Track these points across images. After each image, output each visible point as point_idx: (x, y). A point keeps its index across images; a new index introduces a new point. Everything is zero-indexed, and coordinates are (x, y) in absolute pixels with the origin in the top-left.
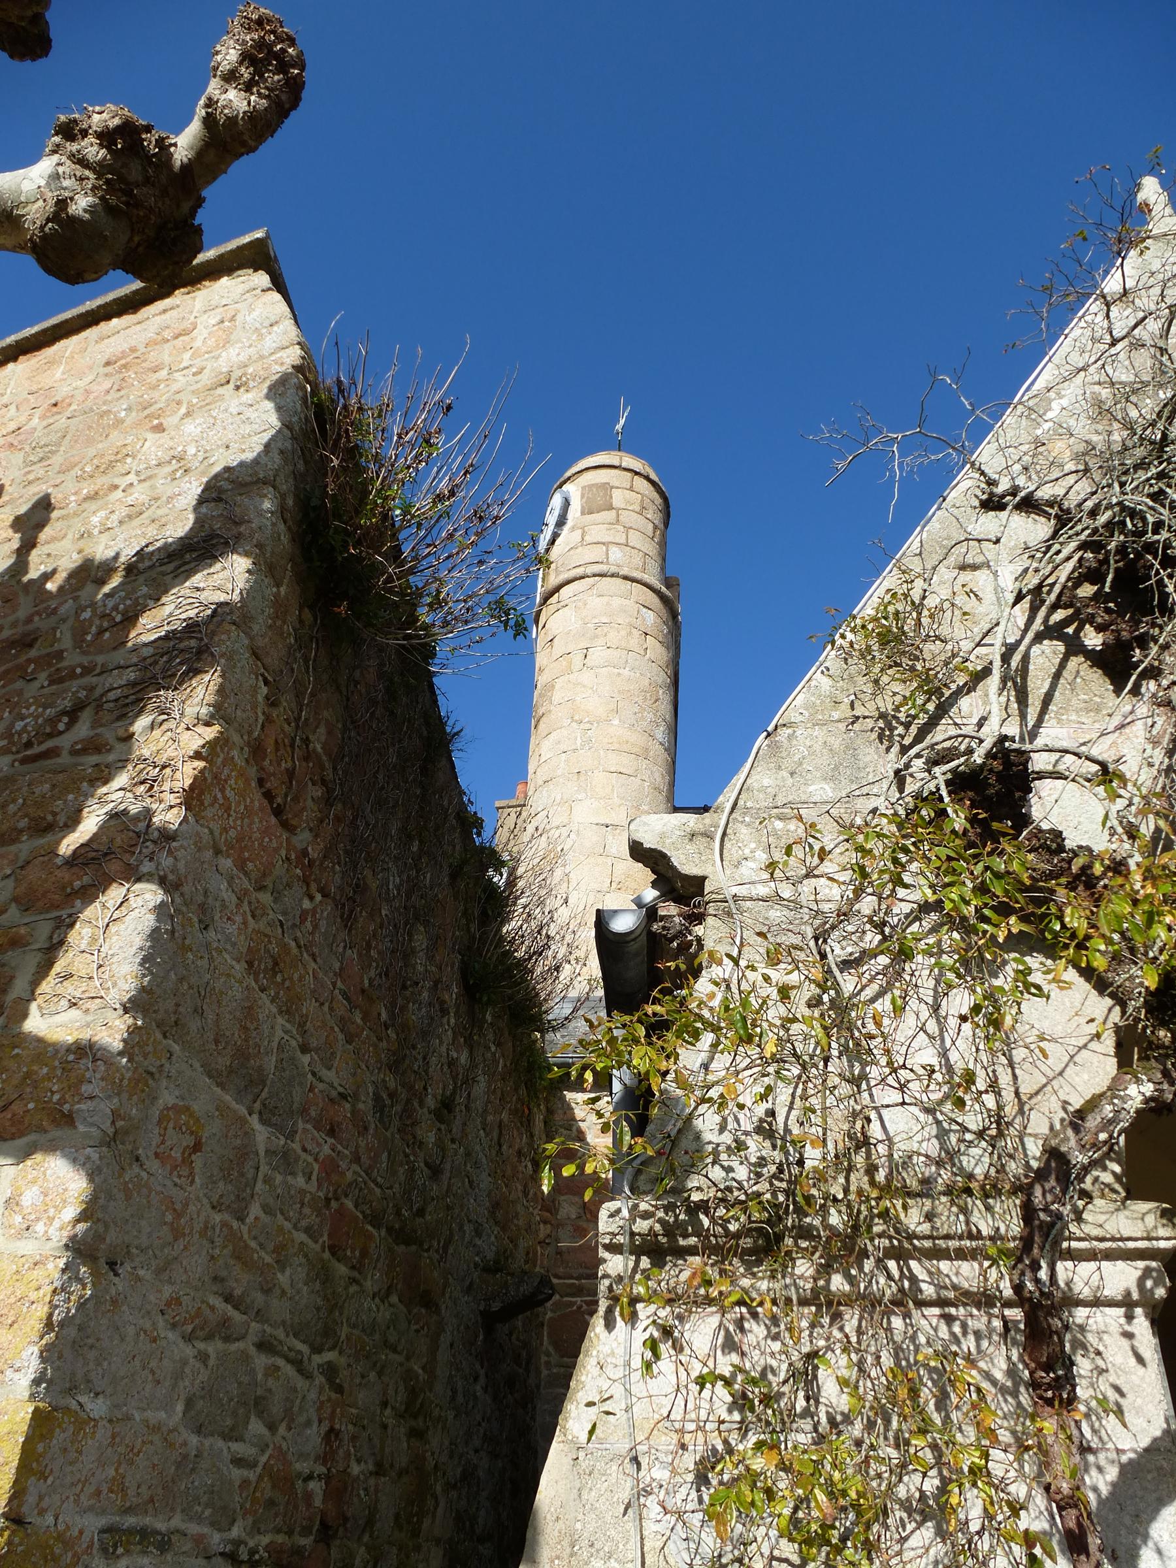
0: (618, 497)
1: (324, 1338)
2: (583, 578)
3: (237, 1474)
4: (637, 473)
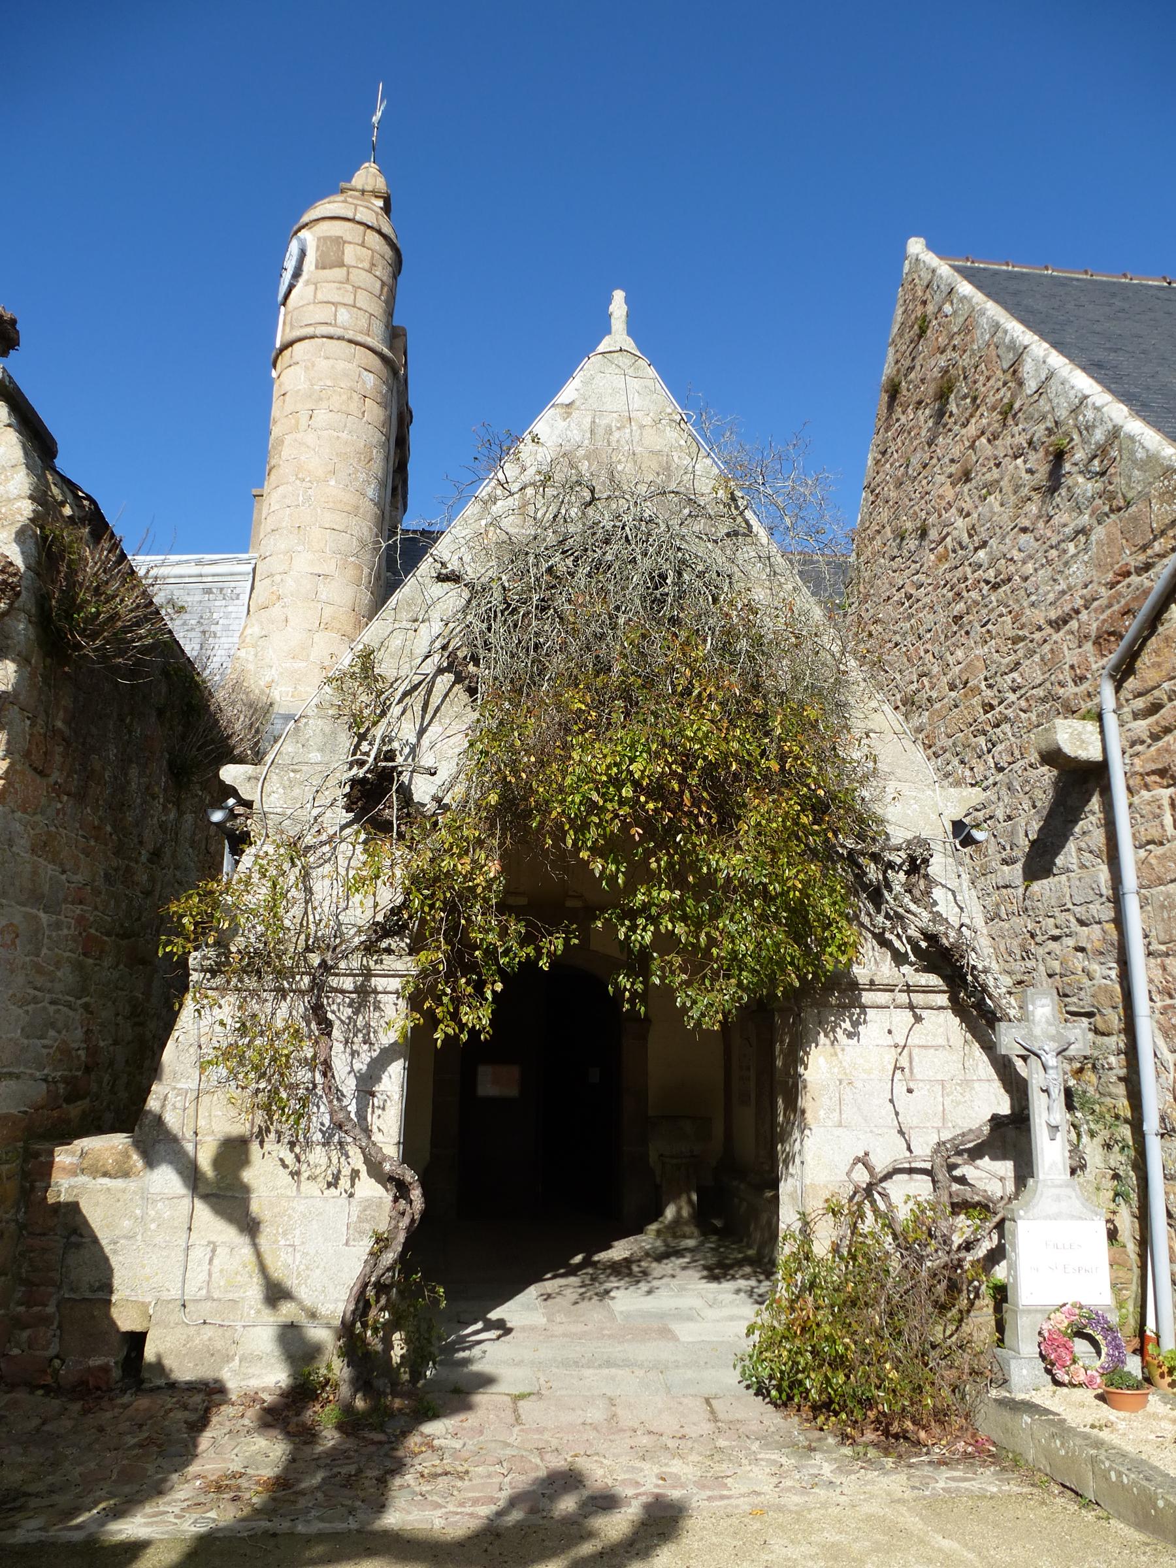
0: (351, 254)
1: (83, 991)
2: (312, 337)
3: (45, 1051)
4: (369, 227)
